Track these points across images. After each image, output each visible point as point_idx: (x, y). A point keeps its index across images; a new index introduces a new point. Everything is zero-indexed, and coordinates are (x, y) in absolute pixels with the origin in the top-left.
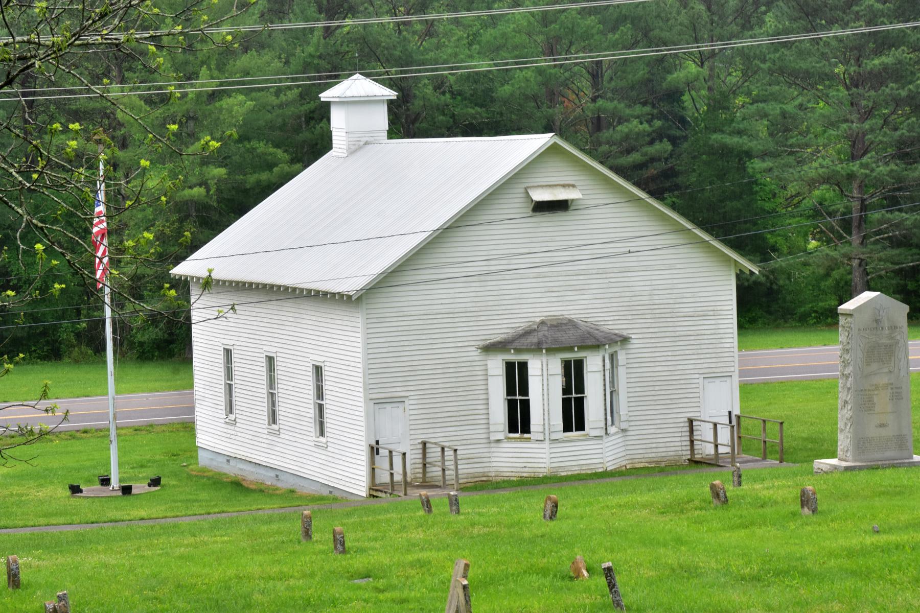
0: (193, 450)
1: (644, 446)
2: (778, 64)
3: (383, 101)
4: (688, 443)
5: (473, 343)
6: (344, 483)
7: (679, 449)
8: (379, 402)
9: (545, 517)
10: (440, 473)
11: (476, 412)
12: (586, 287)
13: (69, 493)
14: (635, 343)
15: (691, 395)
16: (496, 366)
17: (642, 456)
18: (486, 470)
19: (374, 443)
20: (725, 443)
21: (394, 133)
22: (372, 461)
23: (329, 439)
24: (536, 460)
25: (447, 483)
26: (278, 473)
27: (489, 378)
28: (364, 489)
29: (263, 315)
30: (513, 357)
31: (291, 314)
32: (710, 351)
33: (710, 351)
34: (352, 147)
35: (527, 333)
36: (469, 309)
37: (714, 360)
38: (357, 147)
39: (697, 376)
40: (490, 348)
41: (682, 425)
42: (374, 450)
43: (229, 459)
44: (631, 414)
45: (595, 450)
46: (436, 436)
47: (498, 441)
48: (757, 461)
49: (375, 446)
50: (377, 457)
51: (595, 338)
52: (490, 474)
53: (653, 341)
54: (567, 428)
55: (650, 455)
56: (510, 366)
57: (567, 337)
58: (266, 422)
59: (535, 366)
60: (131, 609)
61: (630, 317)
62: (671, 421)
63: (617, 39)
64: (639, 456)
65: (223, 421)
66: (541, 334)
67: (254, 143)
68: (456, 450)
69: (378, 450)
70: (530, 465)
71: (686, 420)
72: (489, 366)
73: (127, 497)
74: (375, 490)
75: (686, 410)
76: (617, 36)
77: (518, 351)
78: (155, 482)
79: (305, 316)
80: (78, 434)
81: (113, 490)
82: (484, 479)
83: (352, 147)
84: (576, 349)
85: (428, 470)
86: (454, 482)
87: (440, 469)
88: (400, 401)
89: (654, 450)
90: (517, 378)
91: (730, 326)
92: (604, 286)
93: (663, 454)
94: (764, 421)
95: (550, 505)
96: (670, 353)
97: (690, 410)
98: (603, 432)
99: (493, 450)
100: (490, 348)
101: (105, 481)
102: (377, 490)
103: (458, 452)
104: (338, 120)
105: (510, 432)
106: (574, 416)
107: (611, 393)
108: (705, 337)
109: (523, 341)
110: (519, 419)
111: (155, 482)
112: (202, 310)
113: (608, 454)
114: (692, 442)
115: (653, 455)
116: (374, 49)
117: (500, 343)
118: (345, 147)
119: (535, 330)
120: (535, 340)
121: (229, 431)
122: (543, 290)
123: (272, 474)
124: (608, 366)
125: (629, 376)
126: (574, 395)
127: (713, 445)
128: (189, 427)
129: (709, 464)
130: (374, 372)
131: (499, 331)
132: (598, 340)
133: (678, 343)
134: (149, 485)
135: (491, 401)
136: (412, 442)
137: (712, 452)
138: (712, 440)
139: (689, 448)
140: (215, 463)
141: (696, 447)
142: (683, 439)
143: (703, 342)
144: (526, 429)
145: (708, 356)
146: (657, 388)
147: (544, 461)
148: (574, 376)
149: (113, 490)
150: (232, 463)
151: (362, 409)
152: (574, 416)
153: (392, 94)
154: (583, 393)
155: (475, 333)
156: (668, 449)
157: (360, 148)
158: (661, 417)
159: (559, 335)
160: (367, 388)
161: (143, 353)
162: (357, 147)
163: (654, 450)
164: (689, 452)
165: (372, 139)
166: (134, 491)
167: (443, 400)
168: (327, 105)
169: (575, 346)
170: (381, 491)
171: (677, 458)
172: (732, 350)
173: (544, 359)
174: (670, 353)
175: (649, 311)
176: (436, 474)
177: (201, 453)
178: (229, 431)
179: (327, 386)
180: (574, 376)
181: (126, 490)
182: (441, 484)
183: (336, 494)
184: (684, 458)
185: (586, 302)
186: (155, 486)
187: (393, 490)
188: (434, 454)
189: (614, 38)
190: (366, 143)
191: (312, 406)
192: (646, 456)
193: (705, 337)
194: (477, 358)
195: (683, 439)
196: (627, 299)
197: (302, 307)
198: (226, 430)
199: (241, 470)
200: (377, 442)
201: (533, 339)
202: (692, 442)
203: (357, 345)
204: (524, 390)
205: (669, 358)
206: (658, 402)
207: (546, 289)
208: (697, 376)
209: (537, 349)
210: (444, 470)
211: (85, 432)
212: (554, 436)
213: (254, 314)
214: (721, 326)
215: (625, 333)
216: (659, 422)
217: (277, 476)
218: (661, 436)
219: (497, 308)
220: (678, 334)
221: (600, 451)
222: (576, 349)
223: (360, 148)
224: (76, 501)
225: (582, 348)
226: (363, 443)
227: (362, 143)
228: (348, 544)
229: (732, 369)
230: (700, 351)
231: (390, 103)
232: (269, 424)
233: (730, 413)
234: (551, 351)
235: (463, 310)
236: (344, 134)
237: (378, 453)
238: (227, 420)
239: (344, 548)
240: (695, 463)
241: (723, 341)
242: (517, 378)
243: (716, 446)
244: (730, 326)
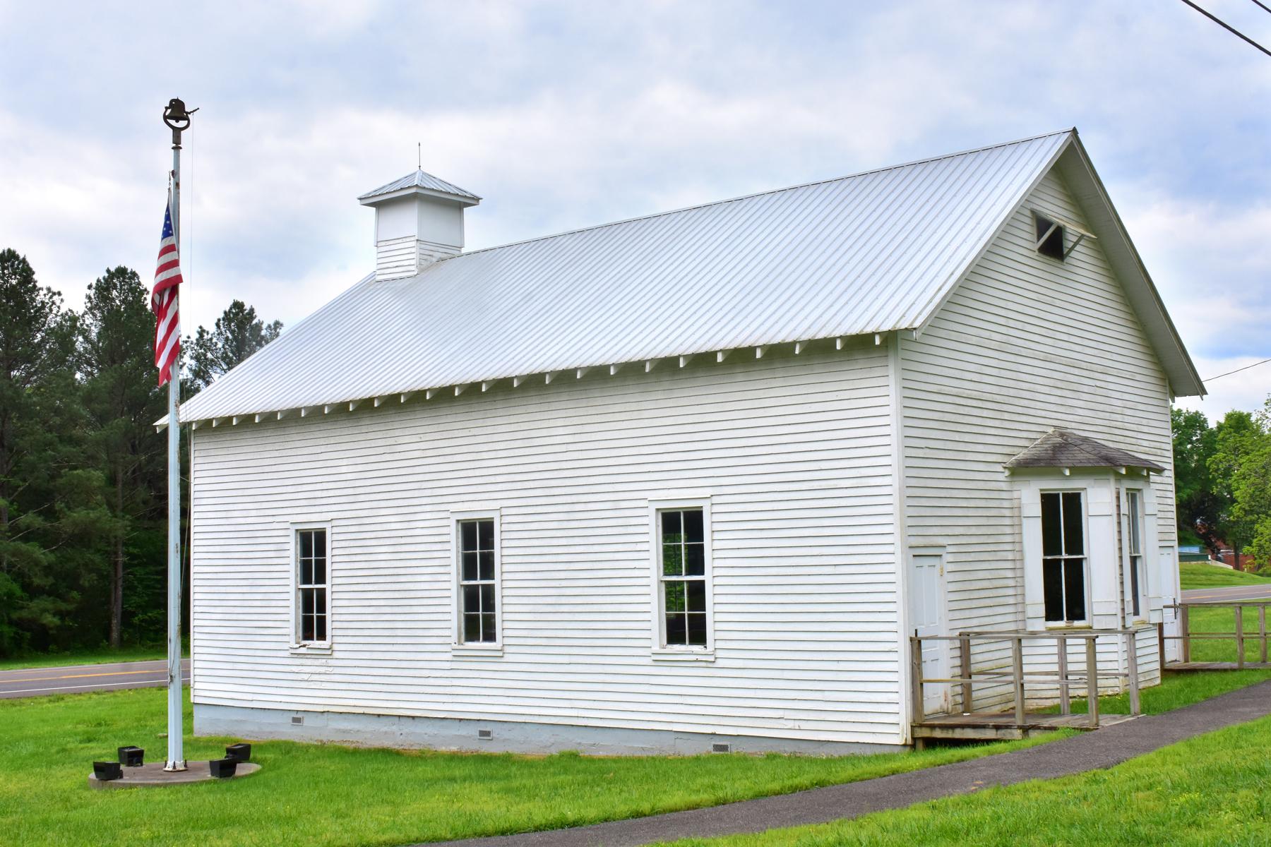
16: (1029, 497)
20: (944, 633)
27: (1024, 520)
31: (560, 422)
40: (1022, 469)
56: (1049, 501)
58: (454, 638)
59: (1099, 503)
72: (1023, 501)
73: (225, 784)
79: (401, 440)
90: (1062, 522)
100: (1022, 469)
107: (1134, 560)
123: (473, 731)
124: (1125, 508)
126: (1064, 556)
150: (308, 721)
199: (344, 731)
203: (1164, 446)
204: (1076, 544)
222: (1067, 473)
227: (434, 260)
236: (414, 244)
242: (1062, 522)
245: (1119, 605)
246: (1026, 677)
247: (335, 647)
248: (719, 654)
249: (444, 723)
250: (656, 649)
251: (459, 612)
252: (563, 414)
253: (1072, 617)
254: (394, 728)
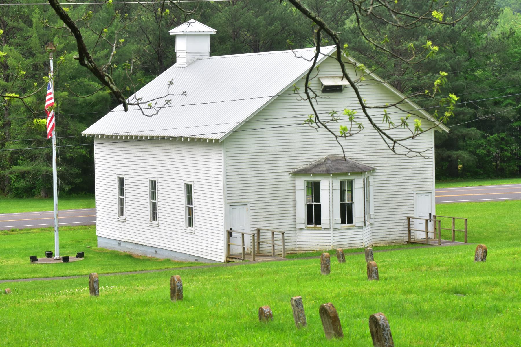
0: (95, 238)
1: (382, 234)
2: (358, 44)
3: (207, 35)
4: (407, 232)
5: (287, 170)
6: (207, 254)
7: (402, 235)
8: (232, 206)
9: (476, 259)
10: (271, 248)
11: (288, 212)
13: (29, 261)
14: (378, 172)
15: (409, 204)
16: (301, 183)
17: (381, 239)
18: (293, 246)
19: (229, 230)
21: (214, 52)
22: (228, 241)
23: (196, 228)
24: (324, 241)
25: (276, 254)
26: (156, 250)
27: (297, 191)
28: (223, 258)
29: (147, 156)
30: (312, 179)
32: (420, 178)
33: (420, 178)
34: (190, 61)
35: (319, 165)
36: (285, 150)
37: (422, 183)
38: (193, 61)
39: (412, 192)
40: (297, 173)
41: (404, 221)
42: (230, 234)
43: (120, 243)
44: (376, 214)
45: (358, 236)
46: (265, 226)
47: (301, 229)
48: (449, 242)
49: (230, 231)
50: (231, 238)
51: (359, 168)
52: (296, 249)
53: (388, 171)
54: (343, 222)
55: (386, 239)
56: (309, 185)
57: (344, 167)
58: (149, 220)
59: (325, 184)
60: (1, 334)
61: (376, 157)
62: (398, 219)
63: (273, 29)
64: (380, 239)
65: (116, 220)
66: (327, 165)
67: (82, 79)
68: (283, 234)
69: (231, 233)
70: (320, 244)
71: (406, 218)
72: (296, 184)
73: (66, 264)
74: (230, 258)
75: (406, 212)
76: (273, 27)
77: (315, 175)
78: (81, 255)
80: (9, 232)
81: (56, 259)
82: (292, 252)
83: (190, 61)
84: (349, 174)
85: (260, 246)
86: (282, 253)
87: (271, 245)
88: (244, 204)
89: (388, 236)
91: (431, 163)
92: (362, 138)
93: (393, 238)
94: (454, 219)
95: (481, 251)
96: (397, 179)
97: (409, 212)
98: (363, 225)
99: (298, 234)
100: (297, 173)
101: (50, 255)
102: (232, 258)
103: (285, 235)
104: (180, 45)
106: (347, 215)
108: (417, 169)
109: (317, 169)
110: (314, 215)
111: (81, 255)
112: (101, 154)
113: (365, 237)
114: (409, 231)
115: (388, 239)
116: (145, 31)
117: (303, 170)
118: (185, 61)
119: (323, 163)
120: (325, 169)
121: (121, 226)
122: (327, 139)
123: (153, 250)
125: (375, 191)
127: (425, 233)
128: (93, 225)
129: (423, 244)
130: (230, 187)
131: (302, 163)
132: (361, 169)
133: (402, 173)
134: (77, 257)
135: (297, 206)
136: (251, 229)
137: (425, 237)
138: (425, 230)
139: (407, 235)
140: (110, 245)
141: (412, 234)
142: (404, 229)
143: (416, 172)
144: (318, 221)
145: (418, 180)
146: (390, 199)
147: (329, 241)
149: (56, 259)
150: (123, 244)
151: (222, 209)
152: (347, 215)
153: (213, 31)
155: (288, 164)
156: (396, 235)
157: (194, 62)
158: (393, 216)
159: (338, 166)
160: (227, 196)
161: (17, 194)
162: (193, 61)
163: (388, 236)
164: (407, 237)
165: (201, 57)
166: (70, 260)
167: (270, 204)
168: (173, 38)
169: (347, 172)
170: (236, 258)
171: (400, 241)
172: (432, 177)
173: (330, 179)
174: (397, 179)
175: (386, 154)
176: (269, 248)
177: (99, 240)
178: (121, 226)
179: (195, 196)
181: (66, 259)
182: (272, 254)
183: (200, 261)
184: (405, 241)
185: (351, 147)
186: (80, 257)
187: (244, 257)
188: (266, 236)
189: (271, 29)
190: (198, 59)
191: (184, 209)
192: (384, 239)
193: (417, 169)
194: (289, 179)
195: (404, 229)
196: (374, 146)
197: (177, 149)
198: (118, 226)
199: (129, 248)
200: (231, 229)
201: (323, 168)
202: (409, 231)
205: (397, 182)
206: (391, 208)
208: (412, 192)
209: (326, 173)
210: (274, 245)
211: (13, 231)
212: (336, 226)
213: (141, 155)
214: (426, 163)
215: (373, 166)
216: (391, 219)
217: (156, 252)
218: (392, 227)
219: (301, 149)
220: (402, 167)
221: (361, 235)
222: (349, 174)
223: (194, 62)
224: (34, 266)
225: (353, 173)
226: (223, 230)
227: (195, 59)
228: (380, 275)
229: (432, 188)
230: (414, 178)
231: (212, 37)
232: (151, 221)
233: (430, 214)
234: (335, 175)
235: (282, 150)
236: (185, 54)
237: (231, 236)
238: (120, 219)
239: (378, 277)
240: (412, 243)
241: (427, 172)
242: (315, 190)
243: (427, 233)
244: (431, 163)
245: (363, 219)
246: (275, 242)
247: (127, 219)
248: (196, 231)
249: (148, 247)
250: (185, 228)
251: (150, 210)
252: (159, 151)
253: (316, 224)
254: (139, 248)
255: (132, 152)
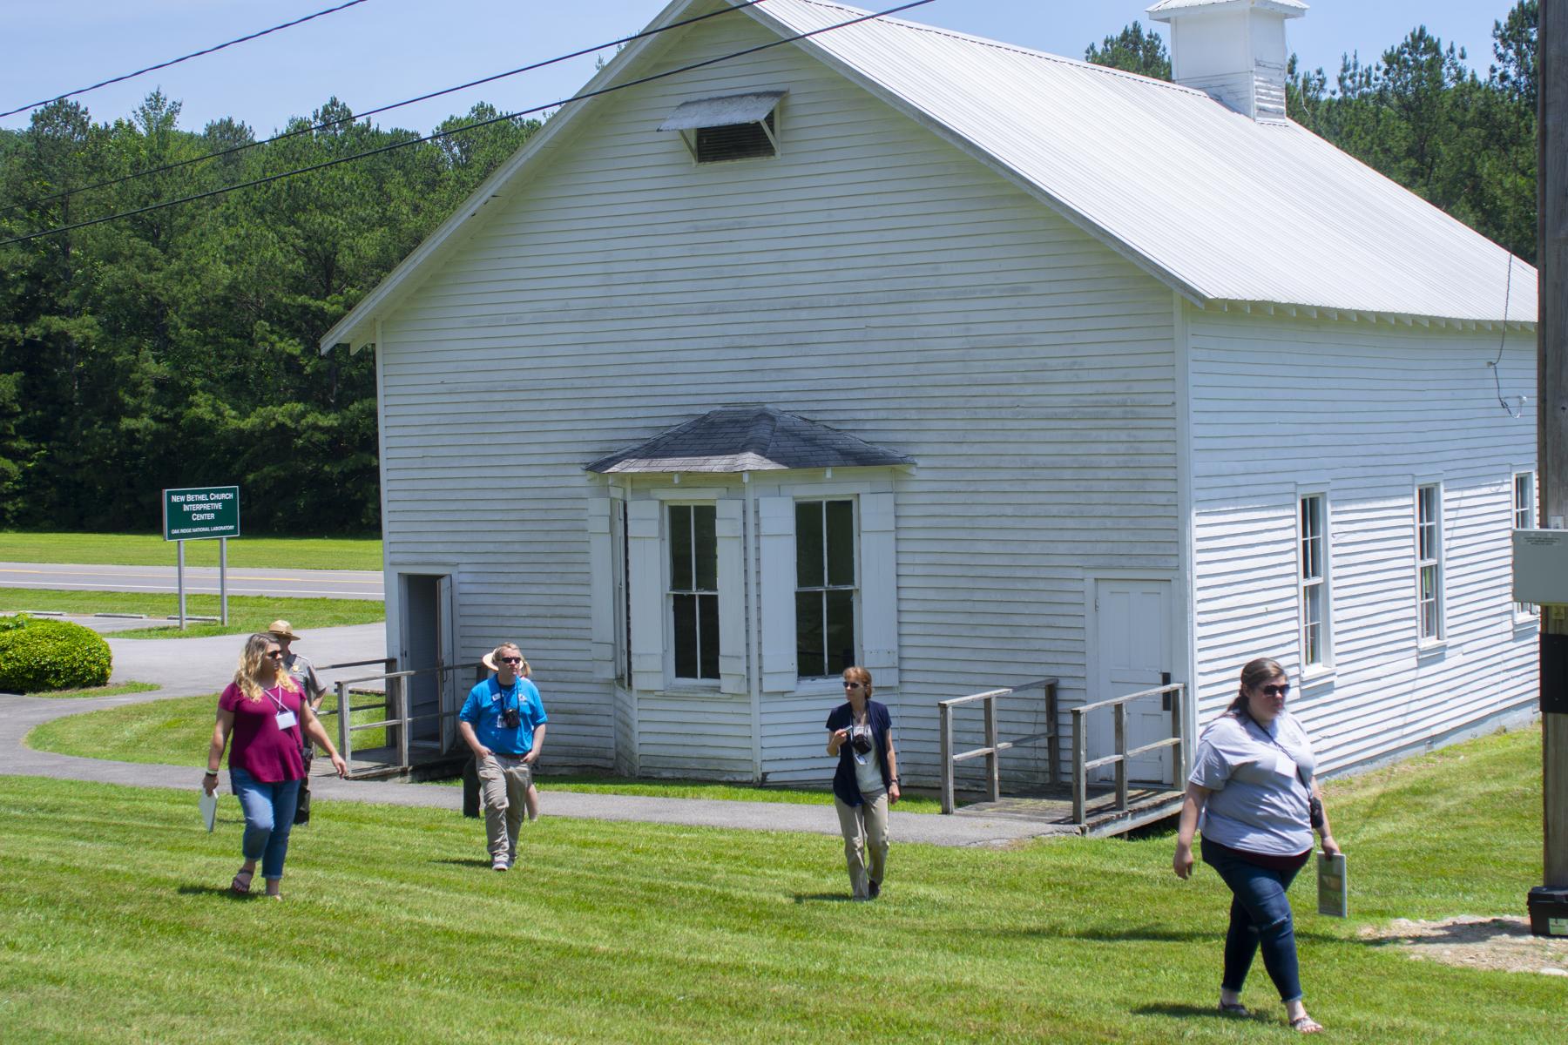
12: (816, 338)
14: (921, 478)
90: (692, 542)
105: (679, 674)
110: (696, 646)
148: (825, 540)
154: (851, 582)
180: (825, 540)
207: (727, 341)
208: (1079, 574)
242: (692, 542)
255: (661, 739)
